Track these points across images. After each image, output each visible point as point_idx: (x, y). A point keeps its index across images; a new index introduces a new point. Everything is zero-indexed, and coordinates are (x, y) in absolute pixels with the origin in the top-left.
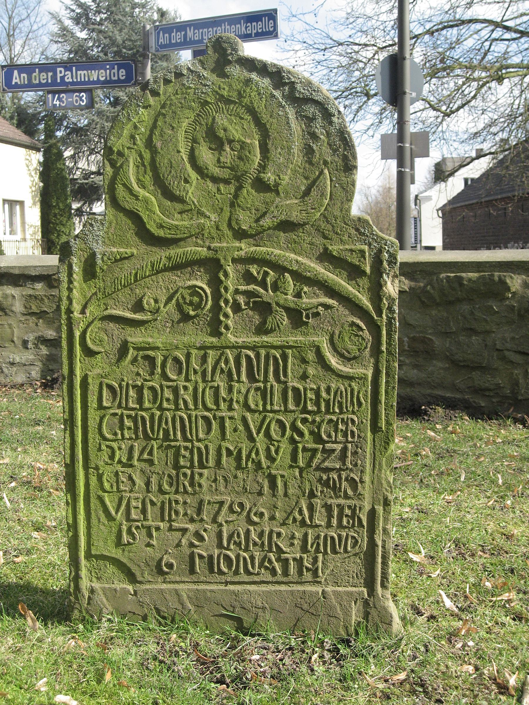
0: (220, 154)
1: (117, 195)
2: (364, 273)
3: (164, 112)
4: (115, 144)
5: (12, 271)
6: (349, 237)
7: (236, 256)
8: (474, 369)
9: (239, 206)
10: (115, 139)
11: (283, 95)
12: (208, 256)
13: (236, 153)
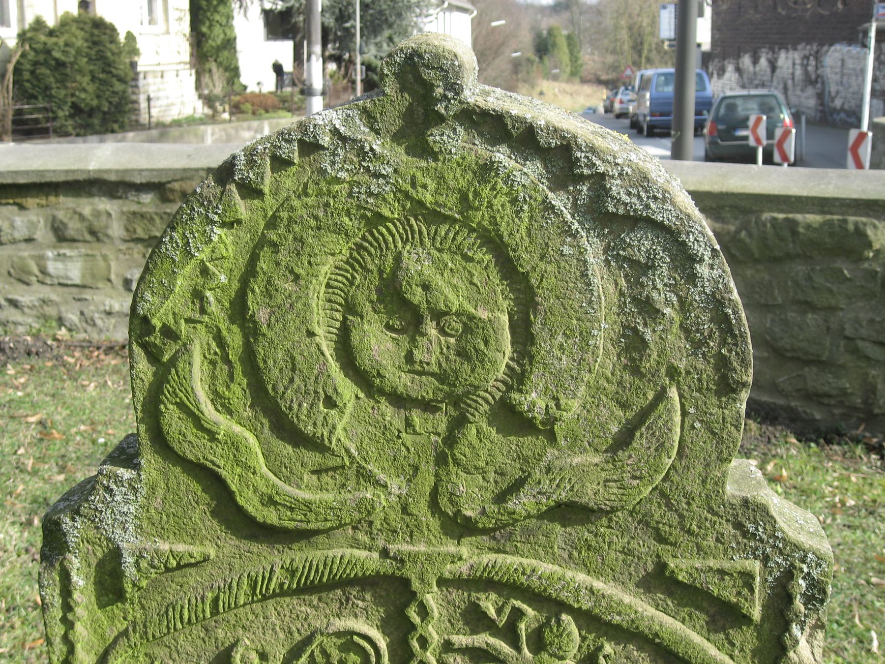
0: (413, 341)
1: (165, 428)
2: (747, 619)
3: (274, 238)
4: (157, 310)
5: (106, 177)
6: (717, 540)
7: (447, 575)
8: (808, 363)
9: (457, 463)
10: (156, 300)
11: (575, 204)
12: (382, 571)
13: (452, 340)
